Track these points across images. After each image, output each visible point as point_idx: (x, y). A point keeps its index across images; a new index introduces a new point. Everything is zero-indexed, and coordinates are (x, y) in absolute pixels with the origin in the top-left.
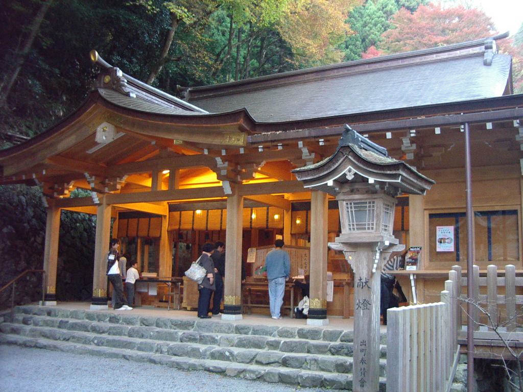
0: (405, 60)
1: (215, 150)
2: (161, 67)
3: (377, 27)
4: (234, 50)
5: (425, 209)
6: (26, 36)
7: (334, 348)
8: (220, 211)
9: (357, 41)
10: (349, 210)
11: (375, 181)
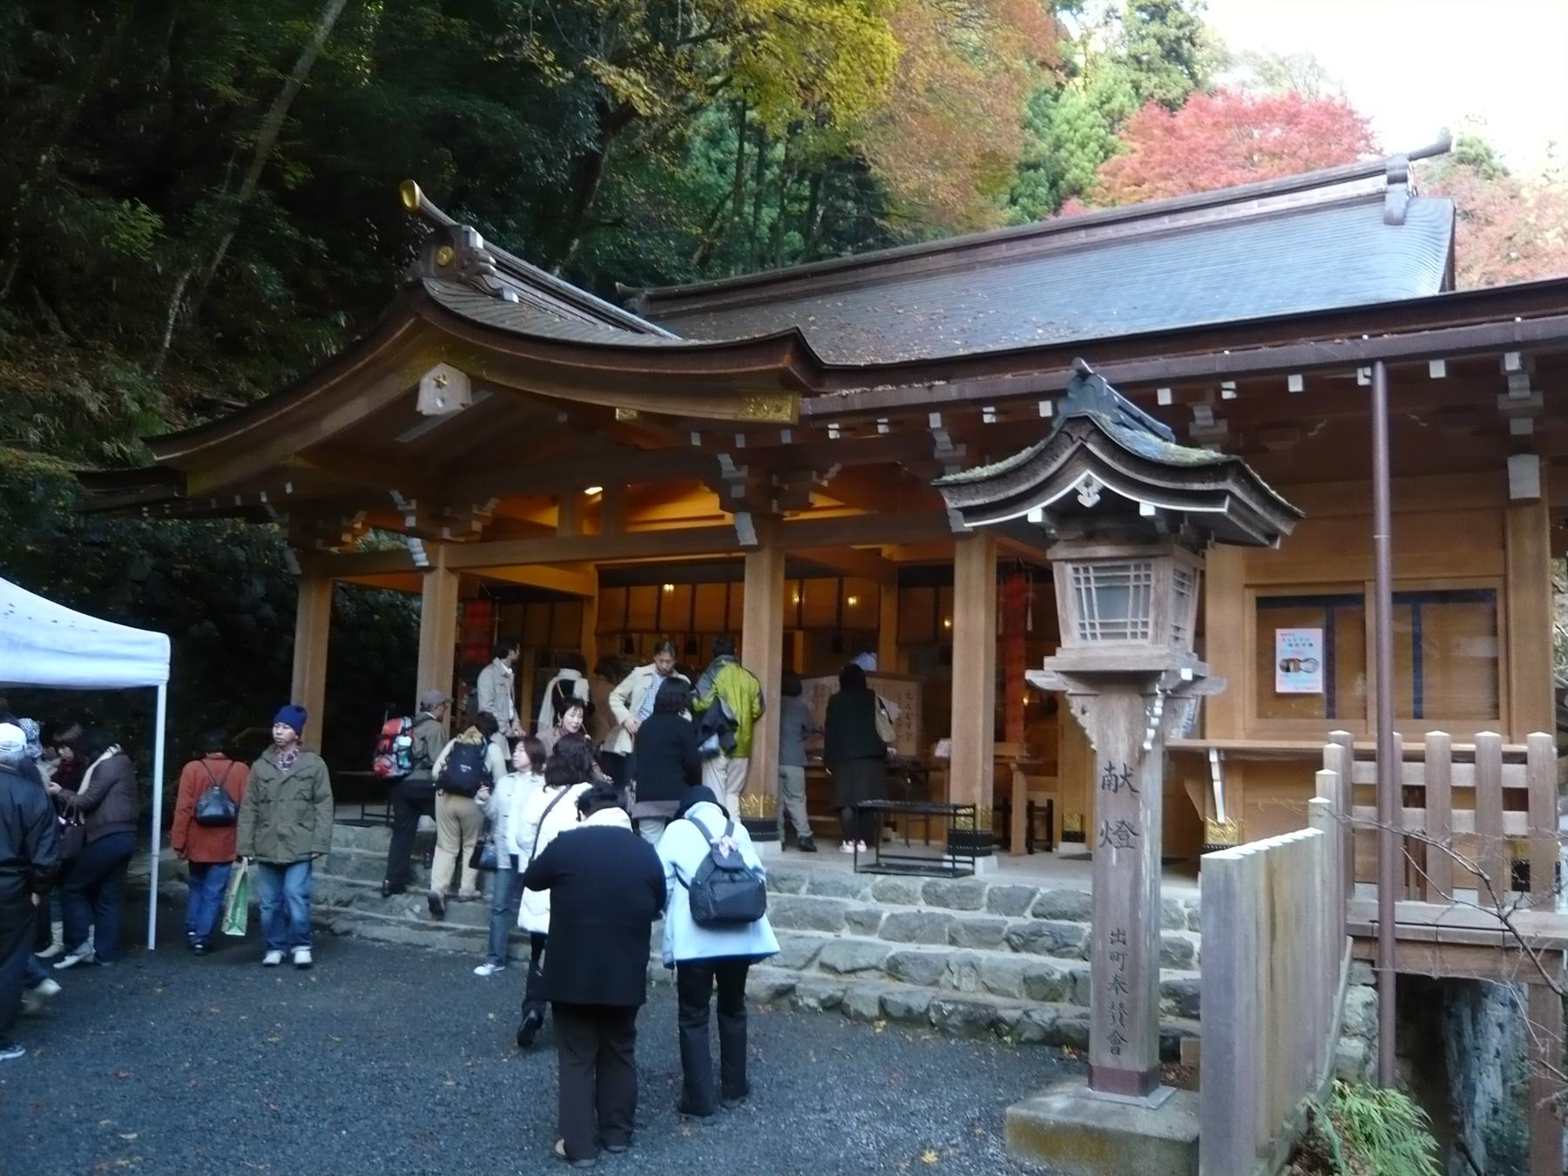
0: (1178, 216)
1: (719, 434)
2: (576, 242)
3: (1086, 150)
4: (748, 209)
5: (1247, 586)
6: (246, 158)
7: (1018, 935)
8: (723, 586)
9: (1037, 186)
10: (1083, 586)
11: (1157, 509)
